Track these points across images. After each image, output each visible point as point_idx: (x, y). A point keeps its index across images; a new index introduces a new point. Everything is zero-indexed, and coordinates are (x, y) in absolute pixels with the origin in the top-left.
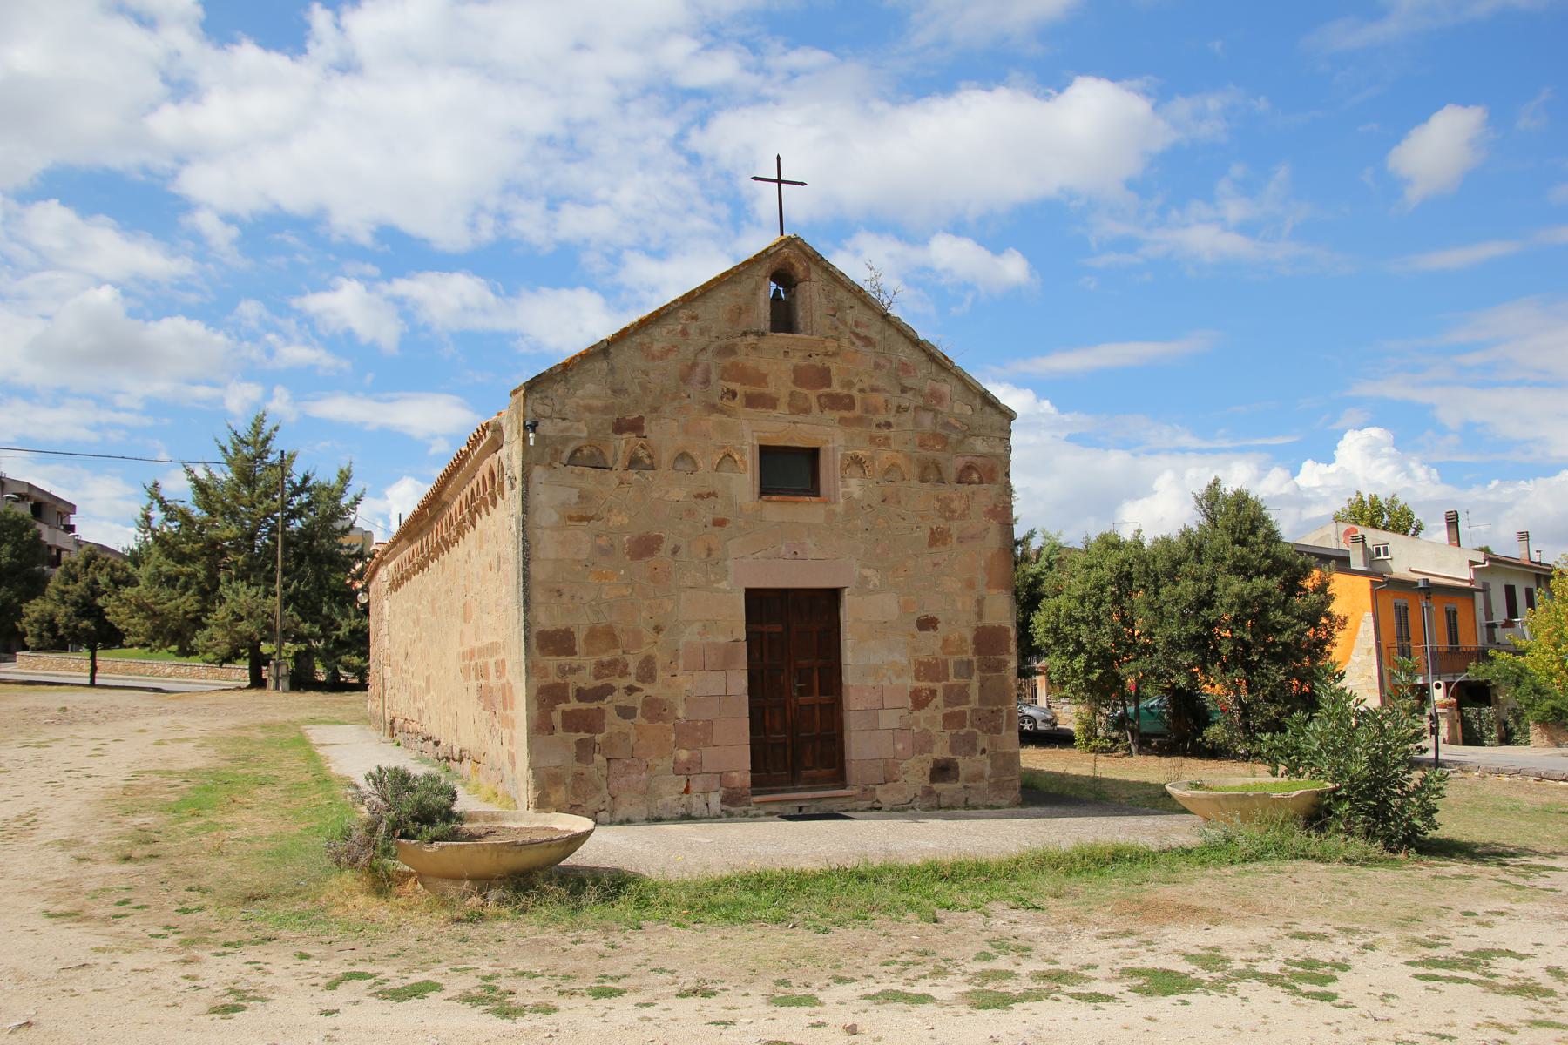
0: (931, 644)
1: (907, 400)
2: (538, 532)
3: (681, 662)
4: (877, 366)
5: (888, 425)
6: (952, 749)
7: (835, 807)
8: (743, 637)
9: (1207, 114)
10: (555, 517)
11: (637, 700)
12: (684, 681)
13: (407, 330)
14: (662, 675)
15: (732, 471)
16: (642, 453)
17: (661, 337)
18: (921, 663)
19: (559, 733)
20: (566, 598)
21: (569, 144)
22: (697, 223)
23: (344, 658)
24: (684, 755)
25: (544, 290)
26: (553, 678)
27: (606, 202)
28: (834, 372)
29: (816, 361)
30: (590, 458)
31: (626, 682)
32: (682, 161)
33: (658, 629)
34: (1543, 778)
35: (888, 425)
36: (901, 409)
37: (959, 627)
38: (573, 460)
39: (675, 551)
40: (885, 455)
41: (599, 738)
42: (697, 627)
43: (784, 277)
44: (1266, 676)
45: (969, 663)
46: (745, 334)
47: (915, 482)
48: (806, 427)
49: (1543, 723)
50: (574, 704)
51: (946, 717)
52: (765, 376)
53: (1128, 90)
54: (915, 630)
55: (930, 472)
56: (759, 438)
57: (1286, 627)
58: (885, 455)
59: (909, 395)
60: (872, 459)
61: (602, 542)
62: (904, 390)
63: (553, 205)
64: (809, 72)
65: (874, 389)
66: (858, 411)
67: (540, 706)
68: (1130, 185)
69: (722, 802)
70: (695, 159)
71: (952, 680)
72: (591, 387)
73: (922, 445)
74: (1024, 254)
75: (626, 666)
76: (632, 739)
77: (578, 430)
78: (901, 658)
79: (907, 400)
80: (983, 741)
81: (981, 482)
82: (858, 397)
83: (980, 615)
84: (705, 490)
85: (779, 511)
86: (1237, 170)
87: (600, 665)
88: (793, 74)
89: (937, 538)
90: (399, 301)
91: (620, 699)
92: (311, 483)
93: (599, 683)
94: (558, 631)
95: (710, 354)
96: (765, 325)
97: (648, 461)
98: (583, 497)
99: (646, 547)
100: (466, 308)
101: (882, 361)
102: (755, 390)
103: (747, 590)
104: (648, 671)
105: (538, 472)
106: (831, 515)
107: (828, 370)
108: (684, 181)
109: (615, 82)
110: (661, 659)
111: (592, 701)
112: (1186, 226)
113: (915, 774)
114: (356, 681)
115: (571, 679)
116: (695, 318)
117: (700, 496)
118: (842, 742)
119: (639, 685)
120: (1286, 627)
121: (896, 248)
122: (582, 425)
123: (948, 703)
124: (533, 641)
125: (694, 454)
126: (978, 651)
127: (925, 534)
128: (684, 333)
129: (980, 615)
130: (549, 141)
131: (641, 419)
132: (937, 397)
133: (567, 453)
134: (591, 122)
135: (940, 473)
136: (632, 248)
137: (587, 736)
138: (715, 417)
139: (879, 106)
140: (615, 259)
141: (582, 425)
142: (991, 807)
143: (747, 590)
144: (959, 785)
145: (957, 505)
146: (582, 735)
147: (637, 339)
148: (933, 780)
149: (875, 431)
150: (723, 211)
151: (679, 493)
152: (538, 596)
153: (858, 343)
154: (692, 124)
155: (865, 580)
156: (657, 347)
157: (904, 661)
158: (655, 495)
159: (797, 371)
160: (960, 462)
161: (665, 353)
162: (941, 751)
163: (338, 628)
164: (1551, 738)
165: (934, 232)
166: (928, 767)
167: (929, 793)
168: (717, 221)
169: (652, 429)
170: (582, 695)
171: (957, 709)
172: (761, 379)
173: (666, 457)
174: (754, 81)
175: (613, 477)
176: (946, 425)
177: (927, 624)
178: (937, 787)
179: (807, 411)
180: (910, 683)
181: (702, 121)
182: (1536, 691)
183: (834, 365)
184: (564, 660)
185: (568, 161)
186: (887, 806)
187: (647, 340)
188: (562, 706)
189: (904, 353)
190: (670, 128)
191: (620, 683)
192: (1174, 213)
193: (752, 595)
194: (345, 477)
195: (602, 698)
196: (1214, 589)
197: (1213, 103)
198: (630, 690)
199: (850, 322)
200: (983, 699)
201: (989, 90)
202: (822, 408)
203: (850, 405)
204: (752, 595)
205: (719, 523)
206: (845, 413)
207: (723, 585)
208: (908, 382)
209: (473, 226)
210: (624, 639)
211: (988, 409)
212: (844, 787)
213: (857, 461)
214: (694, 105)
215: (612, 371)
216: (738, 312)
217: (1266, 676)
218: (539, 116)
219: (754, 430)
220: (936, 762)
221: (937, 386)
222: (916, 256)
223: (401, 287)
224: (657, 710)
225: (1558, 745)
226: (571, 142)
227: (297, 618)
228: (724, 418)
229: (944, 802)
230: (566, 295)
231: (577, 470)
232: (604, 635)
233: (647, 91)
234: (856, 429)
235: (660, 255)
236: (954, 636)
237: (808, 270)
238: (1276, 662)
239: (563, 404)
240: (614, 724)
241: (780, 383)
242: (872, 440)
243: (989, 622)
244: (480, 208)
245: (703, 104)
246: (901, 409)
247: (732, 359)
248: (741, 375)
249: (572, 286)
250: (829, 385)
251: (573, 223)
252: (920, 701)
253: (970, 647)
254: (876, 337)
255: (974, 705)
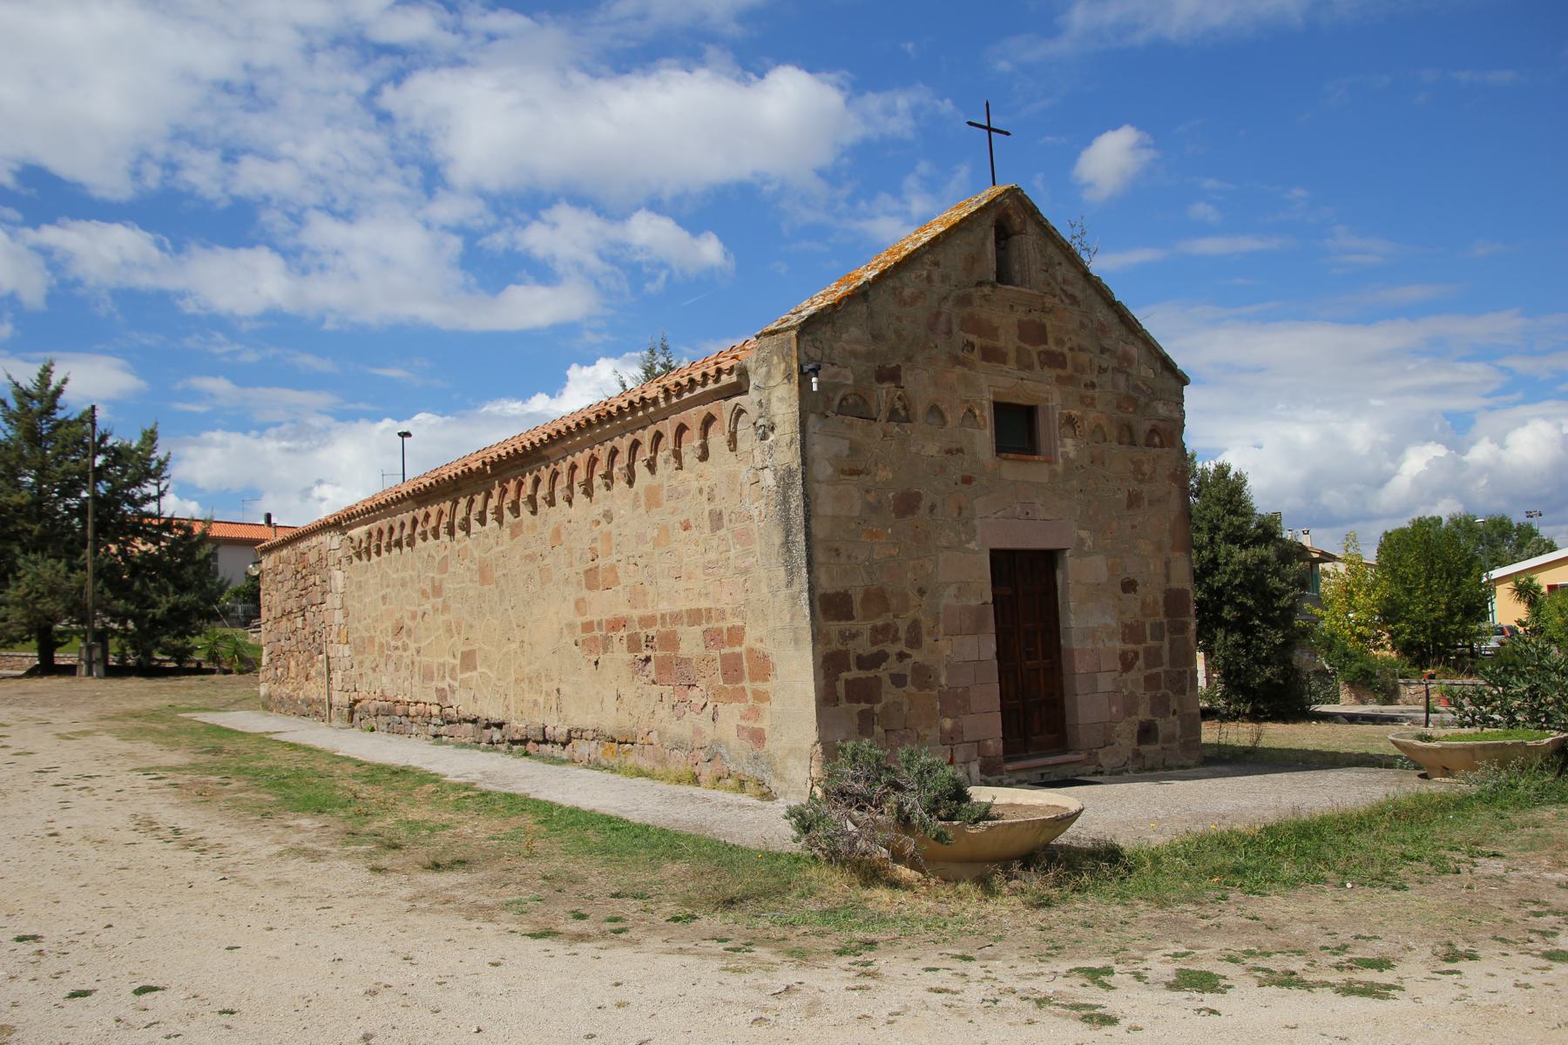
0: (1132, 602)
1: (1107, 361)
2: (816, 486)
3: (941, 626)
4: (1083, 326)
5: (1093, 386)
6: (1153, 712)
7: (1069, 772)
8: (990, 600)
9: (896, 112)
10: (830, 471)
11: (906, 667)
12: (946, 647)
13: (54, 282)
14: (927, 640)
15: (971, 426)
16: (898, 405)
17: (911, 282)
18: (1126, 626)
19: (844, 705)
20: (843, 559)
21: (249, 91)
22: (387, 186)
23: (165, 639)
24: (948, 723)
25: (219, 248)
26: (836, 645)
27: (291, 159)
28: (1049, 328)
29: (1035, 316)
30: (856, 407)
31: (901, 646)
32: (372, 119)
33: (922, 592)
34: (395, 773)
35: (1093, 386)
36: (1102, 370)
37: (1152, 593)
38: (841, 411)
39: (932, 508)
40: (1092, 416)
41: (878, 708)
42: (952, 590)
43: (1003, 233)
44: (1262, 640)
45: (1161, 624)
46: (979, 284)
47: (1115, 443)
48: (1030, 384)
49: (1352, 684)
50: (855, 673)
51: (1147, 679)
52: (996, 329)
53: (823, 82)
54: (1120, 593)
55: (1127, 435)
56: (995, 393)
57: (1283, 593)
58: (1092, 416)
59: (1106, 356)
60: (1082, 419)
61: (871, 498)
62: (1103, 350)
63: (231, 155)
64: (506, 36)
65: (1081, 349)
66: (1069, 370)
67: (827, 676)
68: (821, 173)
69: (981, 771)
70: (385, 117)
71: (1150, 643)
72: (854, 332)
73: (1119, 407)
74: (721, 238)
75: (897, 631)
76: (905, 708)
77: (846, 378)
78: (1110, 621)
79: (1107, 361)
80: (1174, 705)
81: (1162, 446)
82: (1069, 355)
83: (1168, 578)
84: (954, 446)
85: (1013, 470)
86: (923, 167)
87: (875, 630)
88: (491, 37)
89: (1134, 500)
90: (45, 252)
91: (892, 665)
92: (110, 442)
93: (875, 649)
94: (838, 594)
95: (950, 303)
96: (992, 278)
97: (903, 413)
98: (854, 449)
99: (907, 504)
100: (125, 263)
101: (1086, 321)
102: (989, 343)
103: (992, 551)
104: (915, 641)
105: (812, 418)
106: (1053, 474)
107: (1044, 326)
108: (376, 141)
109: (303, 30)
110: (926, 623)
111: (869, 669)
112: (873, 217)
113: (1126, 741)
114: (173, 665)
115: (851, 645)
116: (937, 264)
117: (949, 452)
118: (1063, 708)
119: (908, 651)
120: (1283, 593)
121: (595, 223)
122: (848, 372)
123: (1148, 666)
124: (817, 604)
125: (943, 407)
126: (1167, 614)
127: (1122, 496)
128: (929, 279)
129: (1168, 578)
130: (227, 87)
131: (898, 367)
132: (1126, 358)
133: (837, 402)
134: (273, 70)
135: (1131, 435)
136: (317, 208)
137: (868, 706)
138: (959, 370)
139: (579, 78)
140: (298, 219)
141: (848, 372)
142: (1182, 767)
143: (992, 551)
144: (1158, 747)
145: (1146, 468)
146: (864, 706)
147: (890, 283)
148: (1140, 742)
149: (1083, 391)
150: (415, 174)
151: (932, 449)
152: (820, 557)
153: (1067, 301)
154: (384, 81)
155: (1082, 541)
156: (907, 292)
157: (1113, 623)
158: (913, 449)
159: (1021, 325)
160: (1146, 426)
161: (915, 299)
162: (1143, 714)
163: (154, 605)
164: (1357, 697)
165: (638, 208)
166: (1136, 729)
167: (1137, 755)
168: (407, 183)
169: (907, 378)
170: (862, 663)
171: (1154, 671)
172: (992, 332)
173: (920, 409)
174: (451, 41)
175: (877, 428)
176: (1136, 388)
177: (1129, 586)
178: (1144, 748)
179: (1030, 367)
180: (1118, 645)
181: (398, 78)
182: (1346, 655)
183: (1049, 322)
184: (844, 624)
185: (248, 110)
186: (1108, 770)
187: (898, 285)
188: (845, 675)
189: (1102, 314)
190: (361, 84)
191: (893, 649)
192: (863, 204)
193: (996, 555)
194: (150, 438)
195: (878, 666)
196: (1215, 558)
197: (902, 101)
198: (902, 656)
199: (1060, 279)
200: (1173, 662)
201: (689, 71)
202: (1042, 365)
203: (1063, 365)
204: (996, 555)
205: (967, 480)
206: (1060, 371)
207: (972, 545)
208: (1107, 343)
209: (136, 174)
210: (894, 602)
211: (1166, 374)
212: (1065, 752)
213: (1070, 421)
214: (386, 62)
215: (871, 315)
216: (973, 260)
217: (1262, 640)
218: (214, 57)
219: (993, 384)
220: (1141, 723)
221: (1128, 348)
222: (614, 232)
223: (50, 235)
224: (924, 676)
225: (1364, 703)
226: (251, 90)
227: (108, 594)
228: (966, 370)
229: (1148, 764)
230: (244, 255)
231: (848, 419)
232: (878, 599)
233: (337, 42)
234: (1070, 389)
235: (347, 216)
236: (1150, 599)
237: (1024, 223)
238: (1273, 627)
239: (832, 348)
240: (890, 693)
241: (1007, 340)
242: (1082, 399)
243: (1174, 585)
244: (145, 155)
245: (403, 61)
246: (1102, 370)
247: (969, 310)
248: (973, 324)
249: (251, 244)
250: (1046, 343)
251: (253, 176)
252: (1127, 663)
253: (1161, 611)
254: (1080, 296)
255: (1166, 667)
